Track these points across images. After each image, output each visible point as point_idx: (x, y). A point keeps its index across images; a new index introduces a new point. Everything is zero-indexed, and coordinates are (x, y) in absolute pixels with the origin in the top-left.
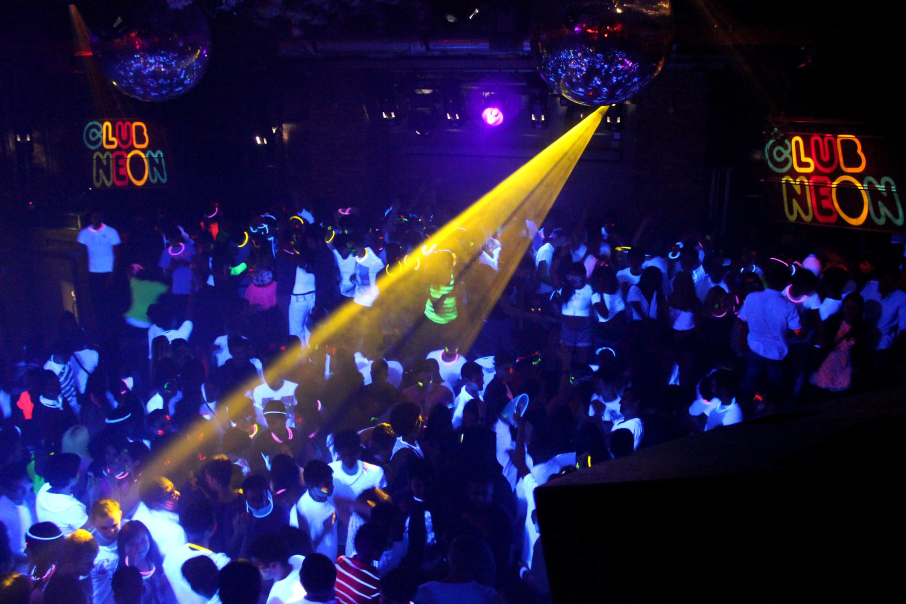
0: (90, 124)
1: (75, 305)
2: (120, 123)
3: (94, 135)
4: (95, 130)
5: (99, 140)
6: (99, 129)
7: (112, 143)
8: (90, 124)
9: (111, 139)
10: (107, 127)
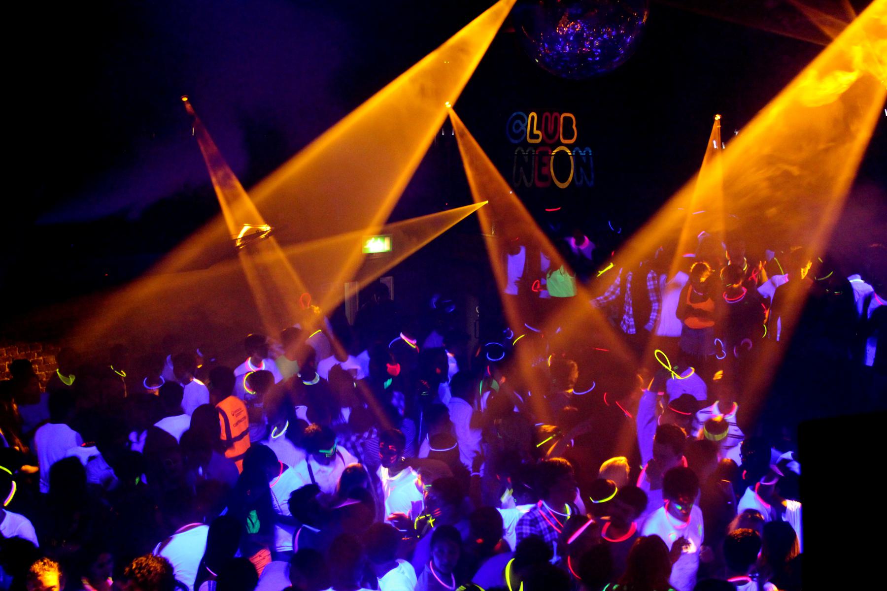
0: (514, 114)
1: (478, 323)
2: (547, 114)
3: (518, 126)
4: (519, 122)
5: (524, 132)
6: (524, 121)
7: (537, 137)
8: (514, 114)
9: (536, 132)
10: (533, 118)
